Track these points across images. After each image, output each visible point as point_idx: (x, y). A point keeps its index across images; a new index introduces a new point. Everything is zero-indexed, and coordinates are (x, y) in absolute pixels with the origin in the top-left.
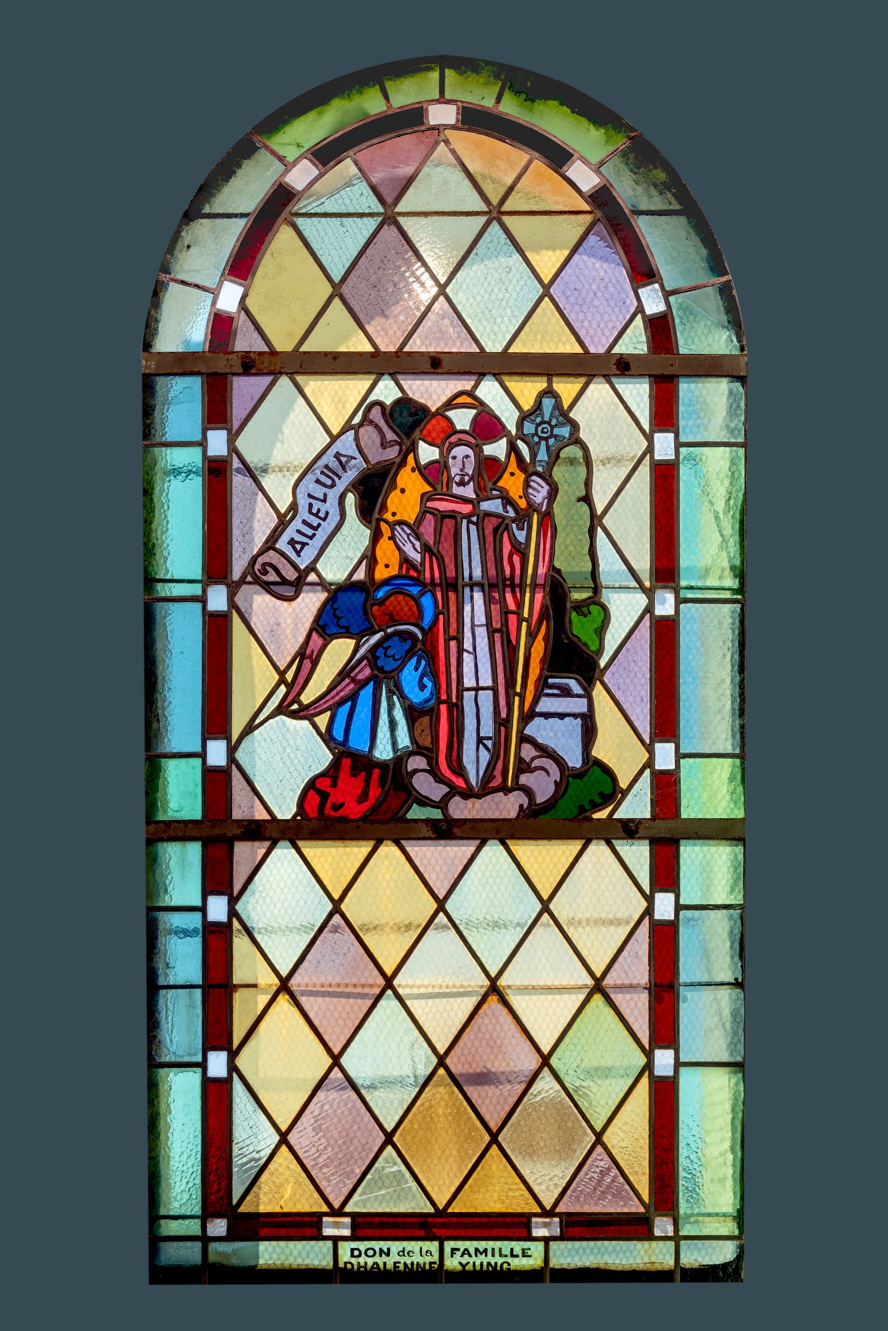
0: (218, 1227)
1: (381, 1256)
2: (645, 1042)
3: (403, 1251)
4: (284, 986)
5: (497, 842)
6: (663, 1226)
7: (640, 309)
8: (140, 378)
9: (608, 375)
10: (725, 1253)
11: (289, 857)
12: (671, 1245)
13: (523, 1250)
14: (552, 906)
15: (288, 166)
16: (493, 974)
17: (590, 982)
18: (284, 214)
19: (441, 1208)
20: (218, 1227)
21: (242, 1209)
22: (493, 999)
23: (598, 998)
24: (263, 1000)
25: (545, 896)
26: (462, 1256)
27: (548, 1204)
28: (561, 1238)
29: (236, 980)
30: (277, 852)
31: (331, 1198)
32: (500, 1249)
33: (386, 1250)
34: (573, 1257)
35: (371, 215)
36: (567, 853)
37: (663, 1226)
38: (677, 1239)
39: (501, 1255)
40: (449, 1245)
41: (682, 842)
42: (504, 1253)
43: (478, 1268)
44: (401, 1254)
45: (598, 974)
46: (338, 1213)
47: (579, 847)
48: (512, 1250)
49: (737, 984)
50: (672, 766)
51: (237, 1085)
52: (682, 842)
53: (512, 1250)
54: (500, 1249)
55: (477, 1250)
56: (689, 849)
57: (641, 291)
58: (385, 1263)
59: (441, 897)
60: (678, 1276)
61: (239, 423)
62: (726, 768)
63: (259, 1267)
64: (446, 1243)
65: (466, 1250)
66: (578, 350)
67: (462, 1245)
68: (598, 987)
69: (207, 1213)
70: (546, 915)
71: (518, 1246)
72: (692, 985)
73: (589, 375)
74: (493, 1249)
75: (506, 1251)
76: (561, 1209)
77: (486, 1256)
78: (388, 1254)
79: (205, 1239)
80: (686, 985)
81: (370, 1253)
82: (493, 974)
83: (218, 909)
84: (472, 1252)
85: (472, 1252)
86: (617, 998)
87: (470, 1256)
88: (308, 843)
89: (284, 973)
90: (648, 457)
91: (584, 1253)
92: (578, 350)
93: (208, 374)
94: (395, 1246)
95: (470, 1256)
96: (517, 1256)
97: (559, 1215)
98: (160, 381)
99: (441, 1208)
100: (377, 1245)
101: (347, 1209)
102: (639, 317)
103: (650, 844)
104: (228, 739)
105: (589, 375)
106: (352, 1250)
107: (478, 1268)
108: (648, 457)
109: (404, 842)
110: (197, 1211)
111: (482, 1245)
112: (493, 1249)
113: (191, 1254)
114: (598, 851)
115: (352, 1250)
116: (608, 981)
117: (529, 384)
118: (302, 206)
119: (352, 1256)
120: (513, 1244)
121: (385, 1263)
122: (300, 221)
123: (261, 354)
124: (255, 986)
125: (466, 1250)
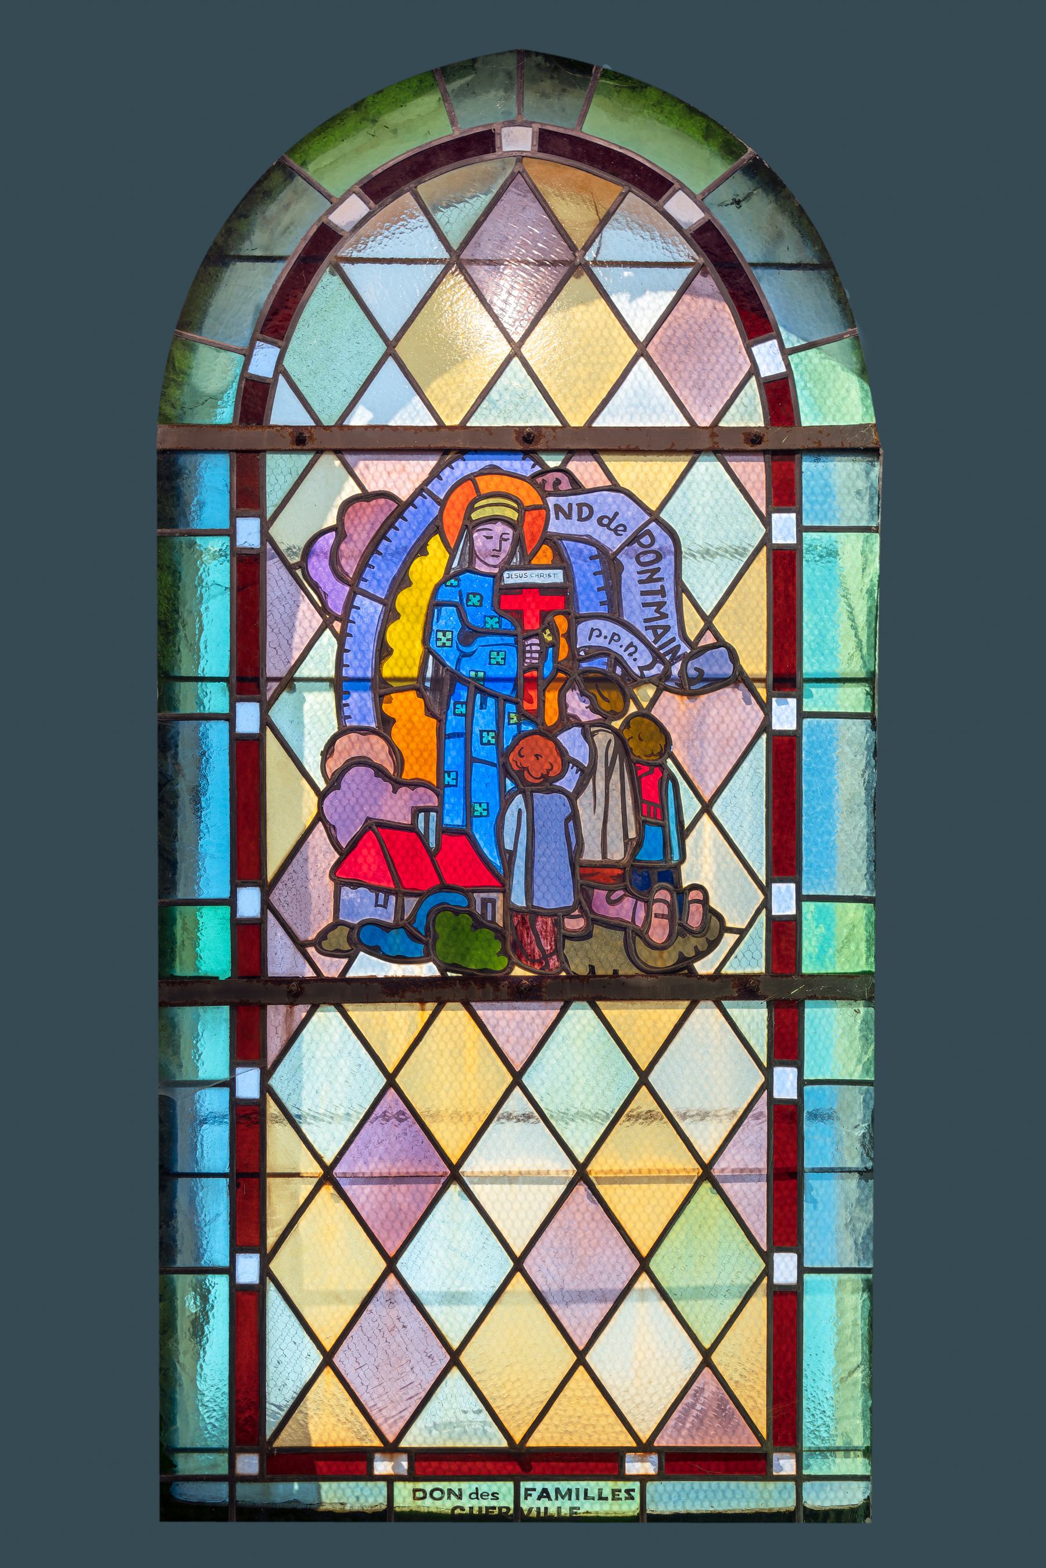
0: (249, 1464)
1: (449, 1498)
2: (764, 1058)
3: (477, 1493)
4: (328, 1176)
5: (459, 1005)
6: (786, 1464)
7: (754, 370)
8: (155, 457)
9: (535, 452)
10: (854, 1495)
11: (712, 1020)
12: (806, 1485)
13: (614, 1491)
14: (509, 1079)
15: (335, 203)
16: (707, 1159)
17: (319, 1171)
18: (330, 257)
19: (644, 1441)
20: (249, 1464)
21: (278, 1443)
22: (581, 1189)
23: (706, 1187)
24: (305, 1189)
25: (643, 1066)
26: (539, 1498)
27: (644, 1436)
28: (659, 1477)
29: (268, 1171)
30: (319, 1016)
31: (384, 1428)
32: (586, 1491)
33: (457, 1492)
34: (702, 1502)
35: (432, 261)
36: (418, 469)
37: (786, 1464)
38: (799, 1479)
39: (586, 1497)
40: (525, 1485)
41: (807, 1002)
42: (590, 1494)
43: (475, 1512)
44: (474, 1496)
45: (581, 1159)
46: (391, 1449)
47: (680, 1012)
48: (600, 1491)
49: (864, 1174)
50: (793, 911)
51: (272, 1293)
52: (808, 1003)
53: (600, 1491)
54: (586, 1491)
55: (557, 1491)
56: (819, 1011)
57: (755, 350)
58: (546, 1509)
59: (518, 1069)
60: (233, 1512)
61: (274, 509)
62: (858, 915)
63: (322, 1508)
64: (522, 1483)
65: (545, 1490)
66: (557, 423)
67: (539, 1485)
68: (707, 1173)
69: (232, 1452)
70: (392, 1090)
71: (607, 1487)
72: (822, 1170)
73: (445, 452)
74: (578, 1490)
75: (593, 1492)
76: (661, 1442)
77: (570, 1499)
78: (460, 1497)
79: (232, 1478)
80: (813, 1170)
81: (437, 1494)
82: (581, 1159)
83: (248, 1084)
84: (553, 1495)
85: (553, 1495)
86: (350, 1190)
87: (550, 1499)
88: (479, 1004)
89: (707, 1158)
90: (765, 1281)
91: (725, 1497)
92: (557, 423)
93: (237, 451)
94: (468, 1487)
95: (550, 1499)
96: (606, 1499)
97: (659, 1451)
98: (185, 460)
99: (644, 1441)
100: (444, 1485)
101: (403, 1444)
102: (753, 379)
103: (768, 1007)
104: (262, 516)
105: (445, 452)
106: (415, 1491)
107: (475, 1512)
108: (765, 1094)
109: (725, 1003)
110: (224, 1441)
111: (564, 1486)
112: (578, 1490)
113: (220, 1493)
114: (706, 1014)
115: (415, 1491)
116: (338, 1170)
117: (422, 463)
118: (345, 251)
119: (415, 1498)
120: (602, 1484)
121: (546, 1509)
122: (347, 267)
123: (554, 428)
124: (297, 1175)
125: (545, 1490)
